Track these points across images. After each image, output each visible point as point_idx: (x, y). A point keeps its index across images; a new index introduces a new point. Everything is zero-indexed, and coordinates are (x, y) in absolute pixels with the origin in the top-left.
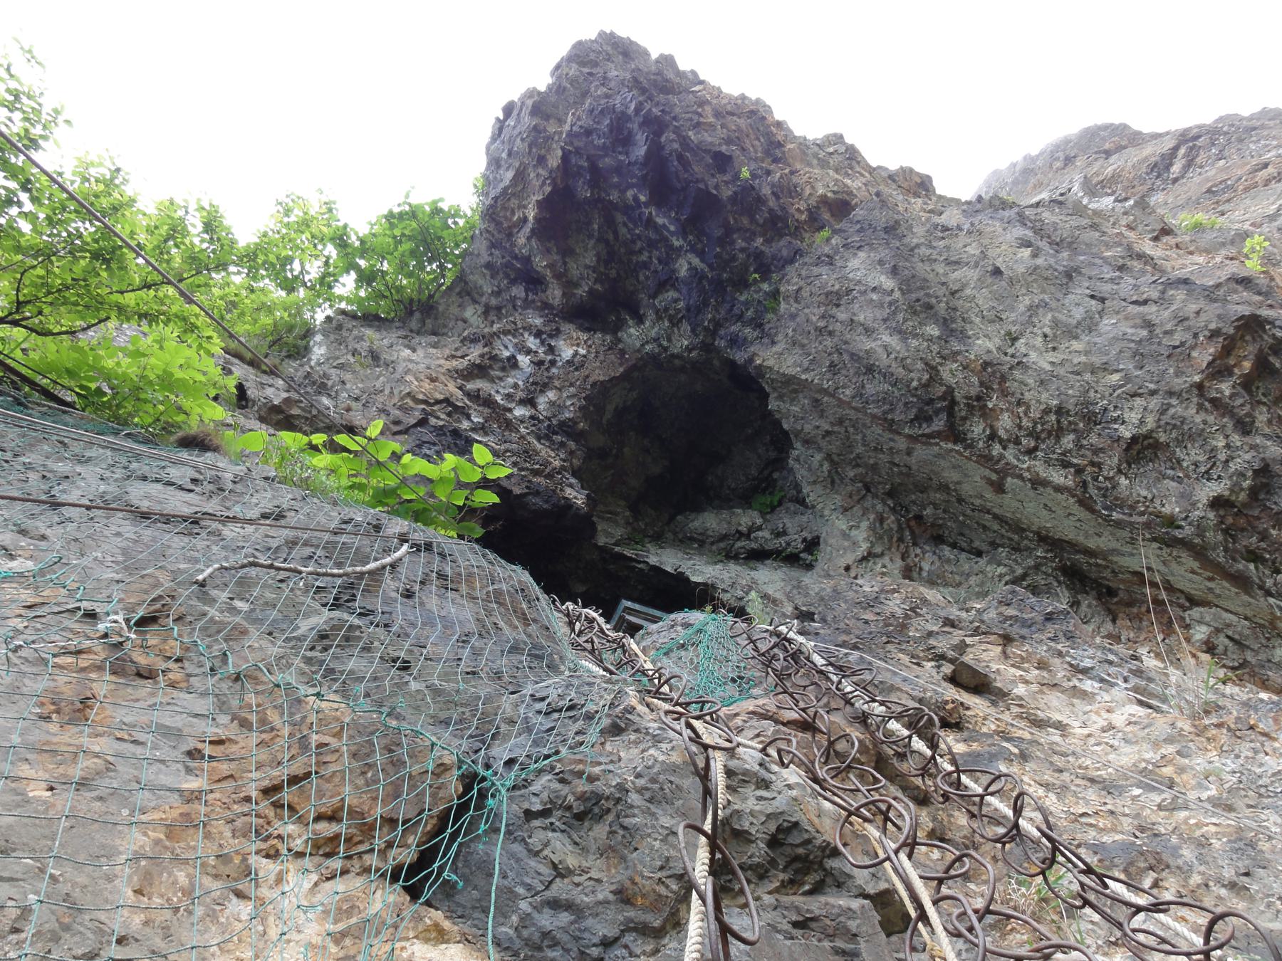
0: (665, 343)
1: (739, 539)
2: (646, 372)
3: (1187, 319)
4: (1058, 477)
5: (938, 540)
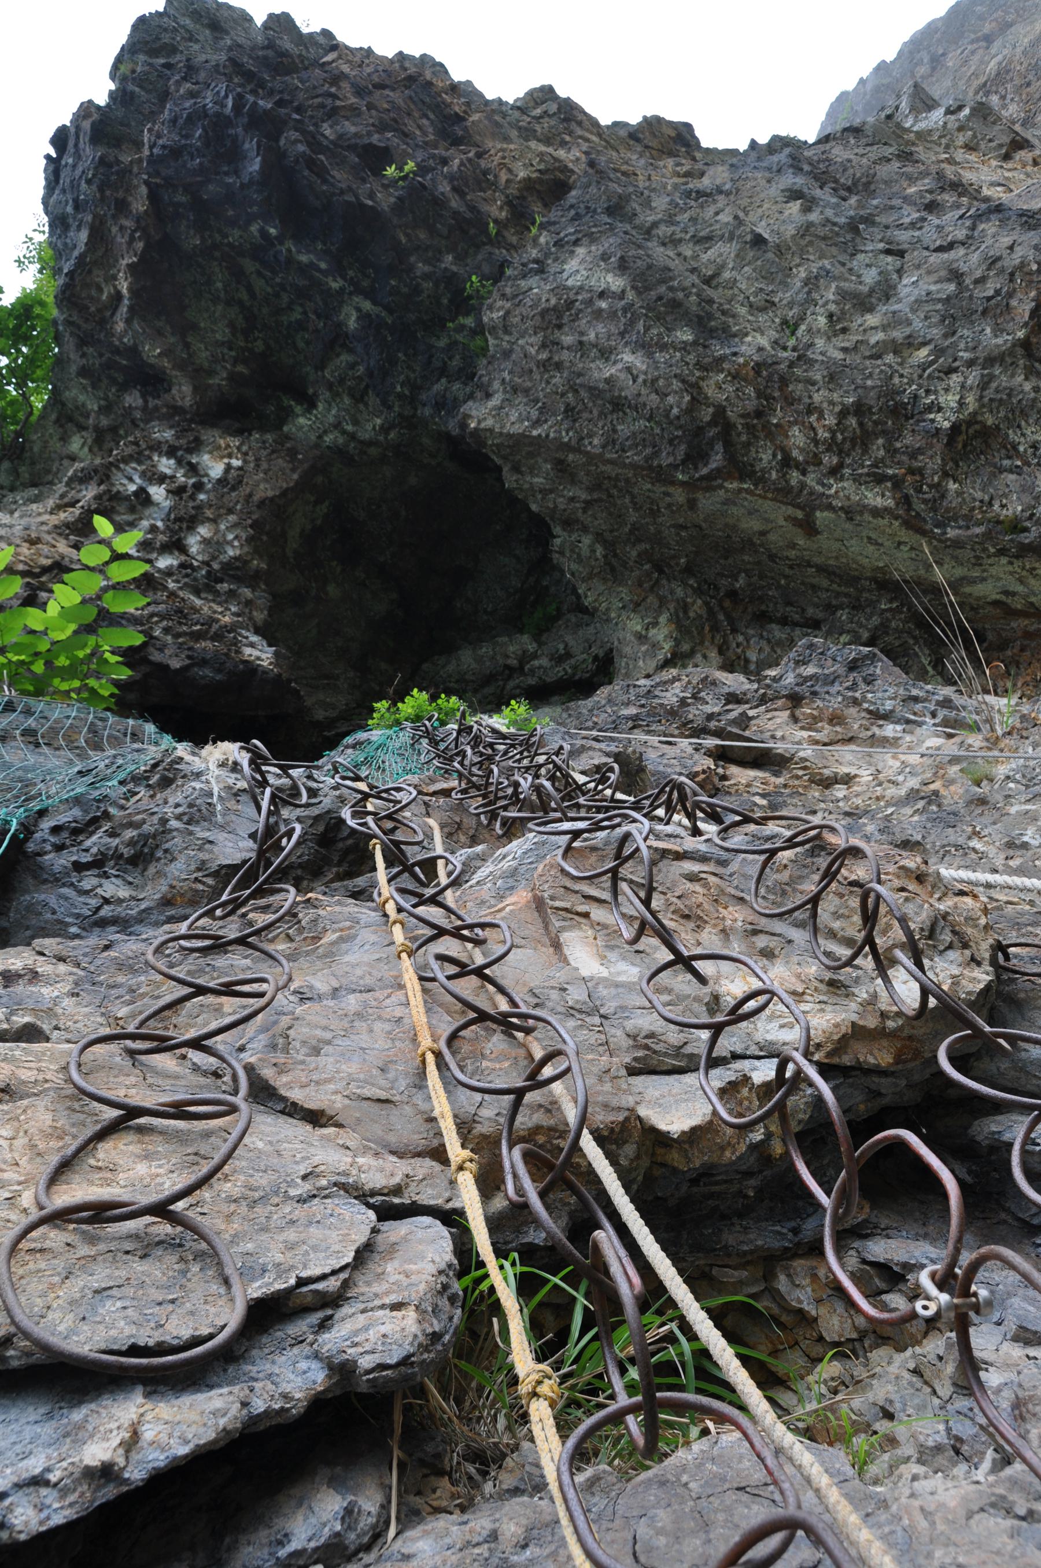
0: (349, 428)
1: (510, 677)
2: (325, 476)
3: (999, 258)
4: (877, 498)
5: (763, 618)
